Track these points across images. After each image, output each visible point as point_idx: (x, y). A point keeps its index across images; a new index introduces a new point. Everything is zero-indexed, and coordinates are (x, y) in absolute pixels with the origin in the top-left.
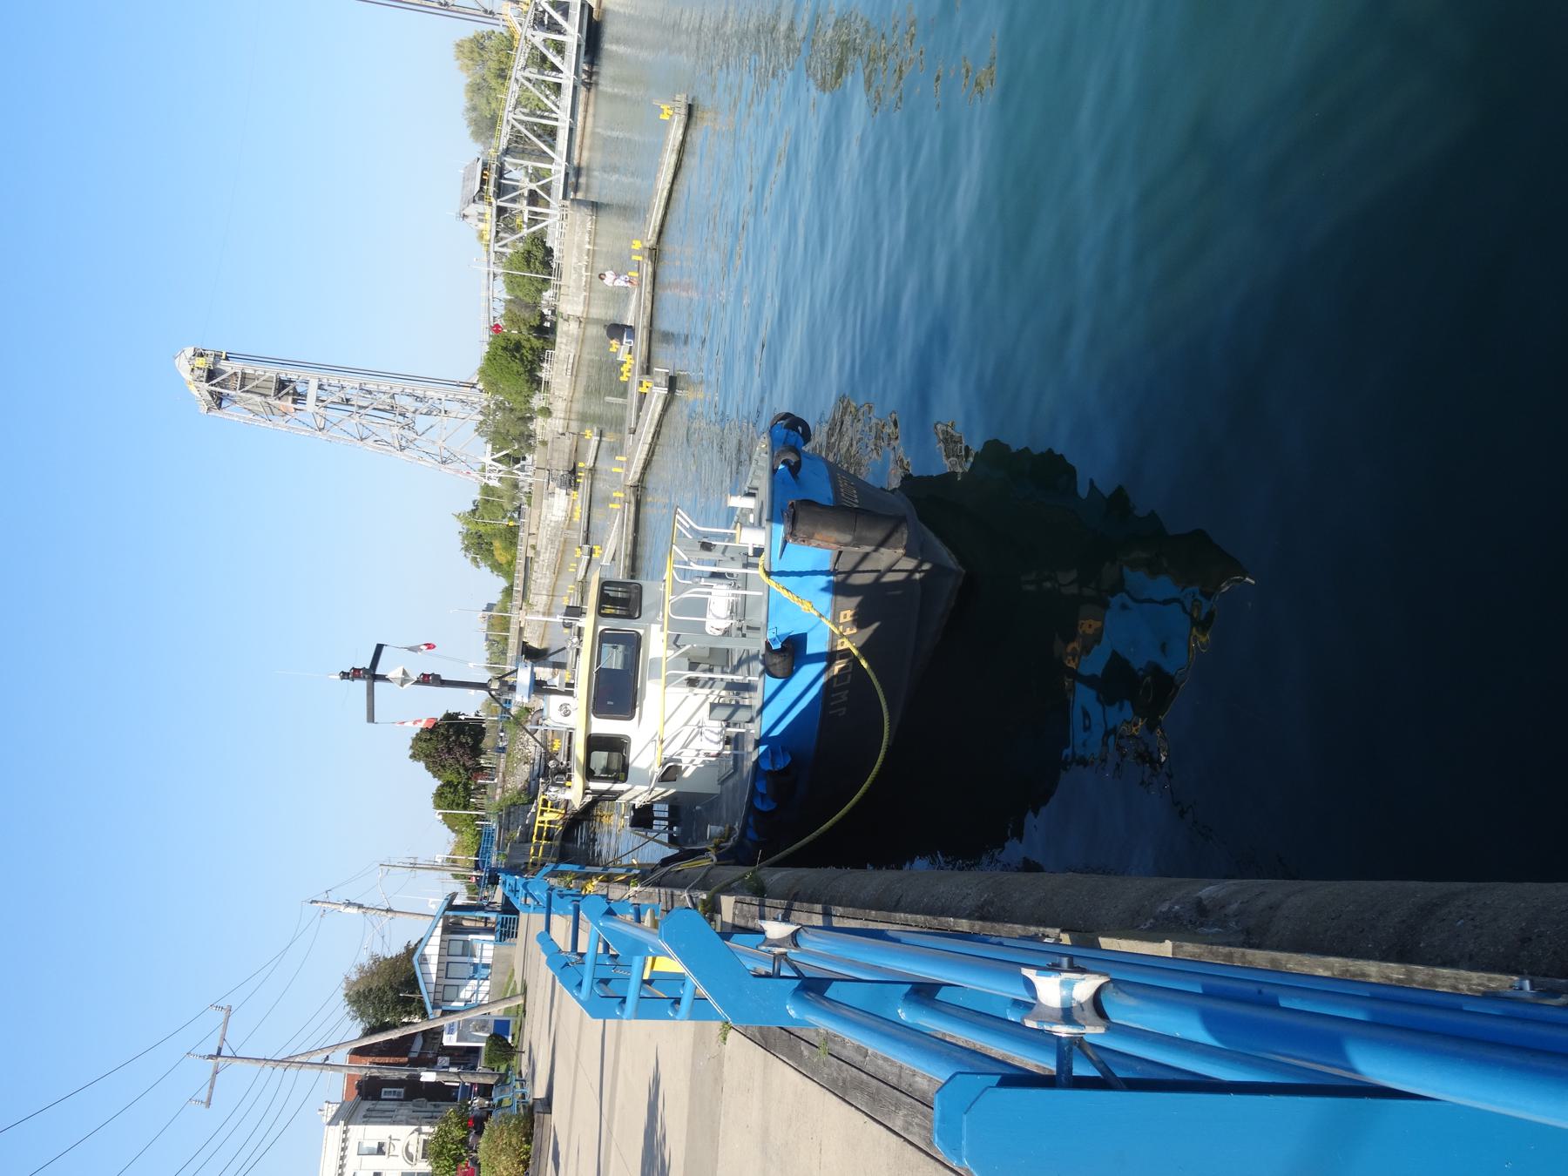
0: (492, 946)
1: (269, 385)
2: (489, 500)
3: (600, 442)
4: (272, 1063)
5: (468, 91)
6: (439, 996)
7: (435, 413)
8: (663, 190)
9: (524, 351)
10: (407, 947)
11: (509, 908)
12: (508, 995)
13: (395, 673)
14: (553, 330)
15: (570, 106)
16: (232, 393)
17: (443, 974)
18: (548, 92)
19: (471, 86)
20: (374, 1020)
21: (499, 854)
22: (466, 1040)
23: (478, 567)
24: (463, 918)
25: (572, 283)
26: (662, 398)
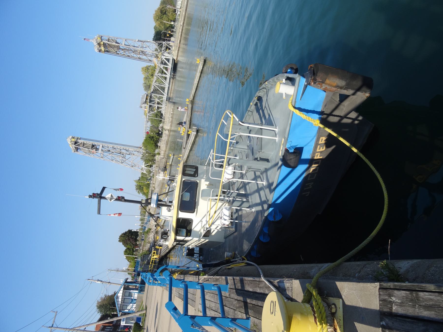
0: (137, 294)
1: (90, 146)
2: (143, 177)
3: (173, 157)
4: (68, 330)
5: (144, 79)
6: (121, 308)
7: (131, 154)
8: (196, 84)
9: (154, 138)
10: (115, 293)
11: (143, 283)
12: (140, 310)
13: (108, 196)
14: (162, 134)
15: (167, 92)
16: (81, 147)
17: (123, 302)
18: (163, 79)
19: (145, 78)
20: (104, 313)
21: (140, 268)
22: (128, 323)
23: (139, 194)
24: (130, 285)
25: (167, 121)
26: (194, 136)
